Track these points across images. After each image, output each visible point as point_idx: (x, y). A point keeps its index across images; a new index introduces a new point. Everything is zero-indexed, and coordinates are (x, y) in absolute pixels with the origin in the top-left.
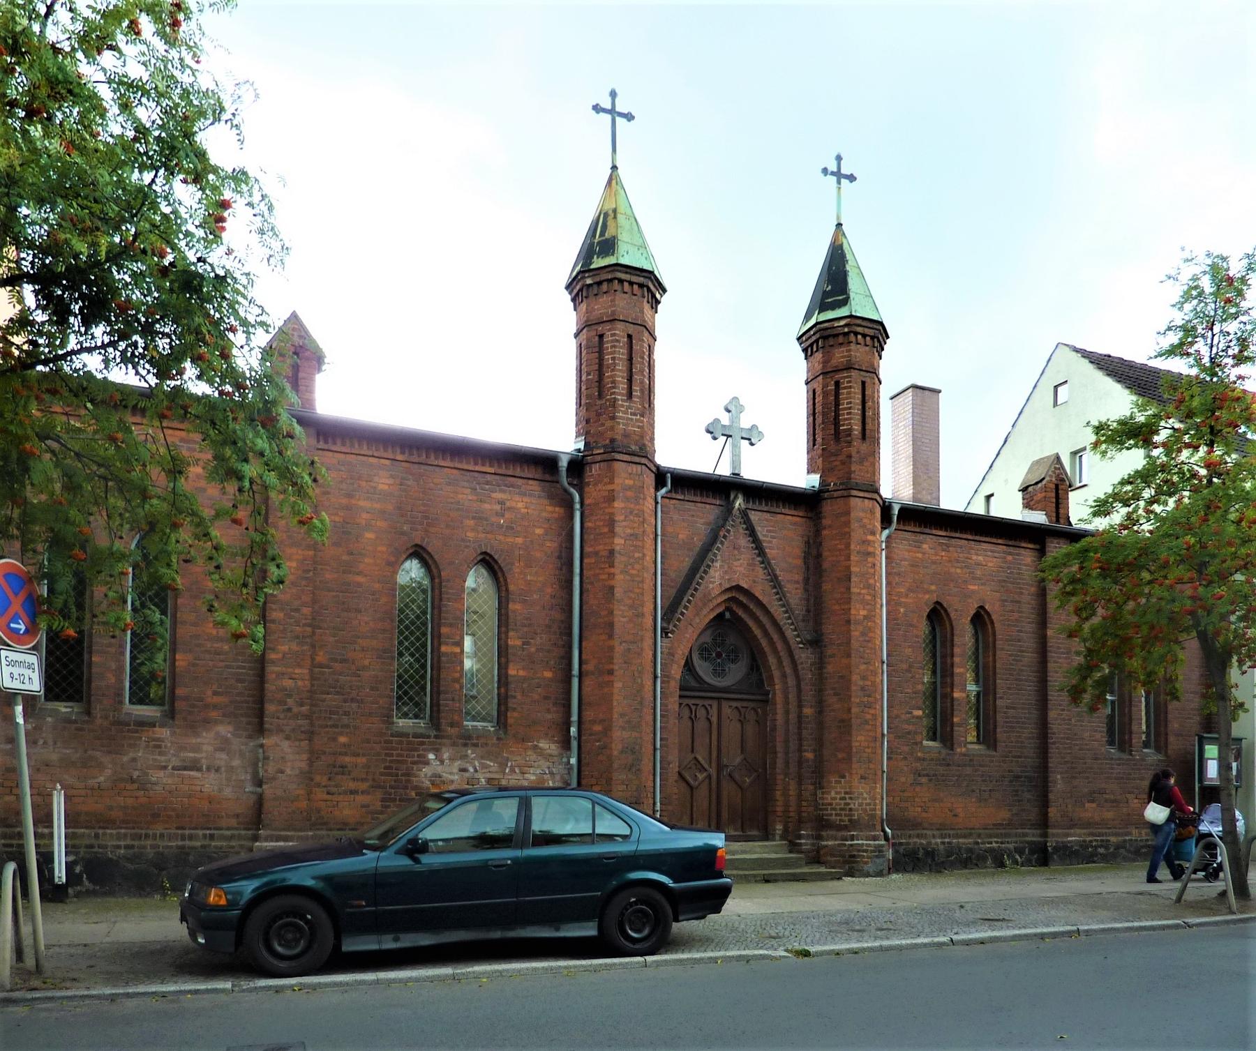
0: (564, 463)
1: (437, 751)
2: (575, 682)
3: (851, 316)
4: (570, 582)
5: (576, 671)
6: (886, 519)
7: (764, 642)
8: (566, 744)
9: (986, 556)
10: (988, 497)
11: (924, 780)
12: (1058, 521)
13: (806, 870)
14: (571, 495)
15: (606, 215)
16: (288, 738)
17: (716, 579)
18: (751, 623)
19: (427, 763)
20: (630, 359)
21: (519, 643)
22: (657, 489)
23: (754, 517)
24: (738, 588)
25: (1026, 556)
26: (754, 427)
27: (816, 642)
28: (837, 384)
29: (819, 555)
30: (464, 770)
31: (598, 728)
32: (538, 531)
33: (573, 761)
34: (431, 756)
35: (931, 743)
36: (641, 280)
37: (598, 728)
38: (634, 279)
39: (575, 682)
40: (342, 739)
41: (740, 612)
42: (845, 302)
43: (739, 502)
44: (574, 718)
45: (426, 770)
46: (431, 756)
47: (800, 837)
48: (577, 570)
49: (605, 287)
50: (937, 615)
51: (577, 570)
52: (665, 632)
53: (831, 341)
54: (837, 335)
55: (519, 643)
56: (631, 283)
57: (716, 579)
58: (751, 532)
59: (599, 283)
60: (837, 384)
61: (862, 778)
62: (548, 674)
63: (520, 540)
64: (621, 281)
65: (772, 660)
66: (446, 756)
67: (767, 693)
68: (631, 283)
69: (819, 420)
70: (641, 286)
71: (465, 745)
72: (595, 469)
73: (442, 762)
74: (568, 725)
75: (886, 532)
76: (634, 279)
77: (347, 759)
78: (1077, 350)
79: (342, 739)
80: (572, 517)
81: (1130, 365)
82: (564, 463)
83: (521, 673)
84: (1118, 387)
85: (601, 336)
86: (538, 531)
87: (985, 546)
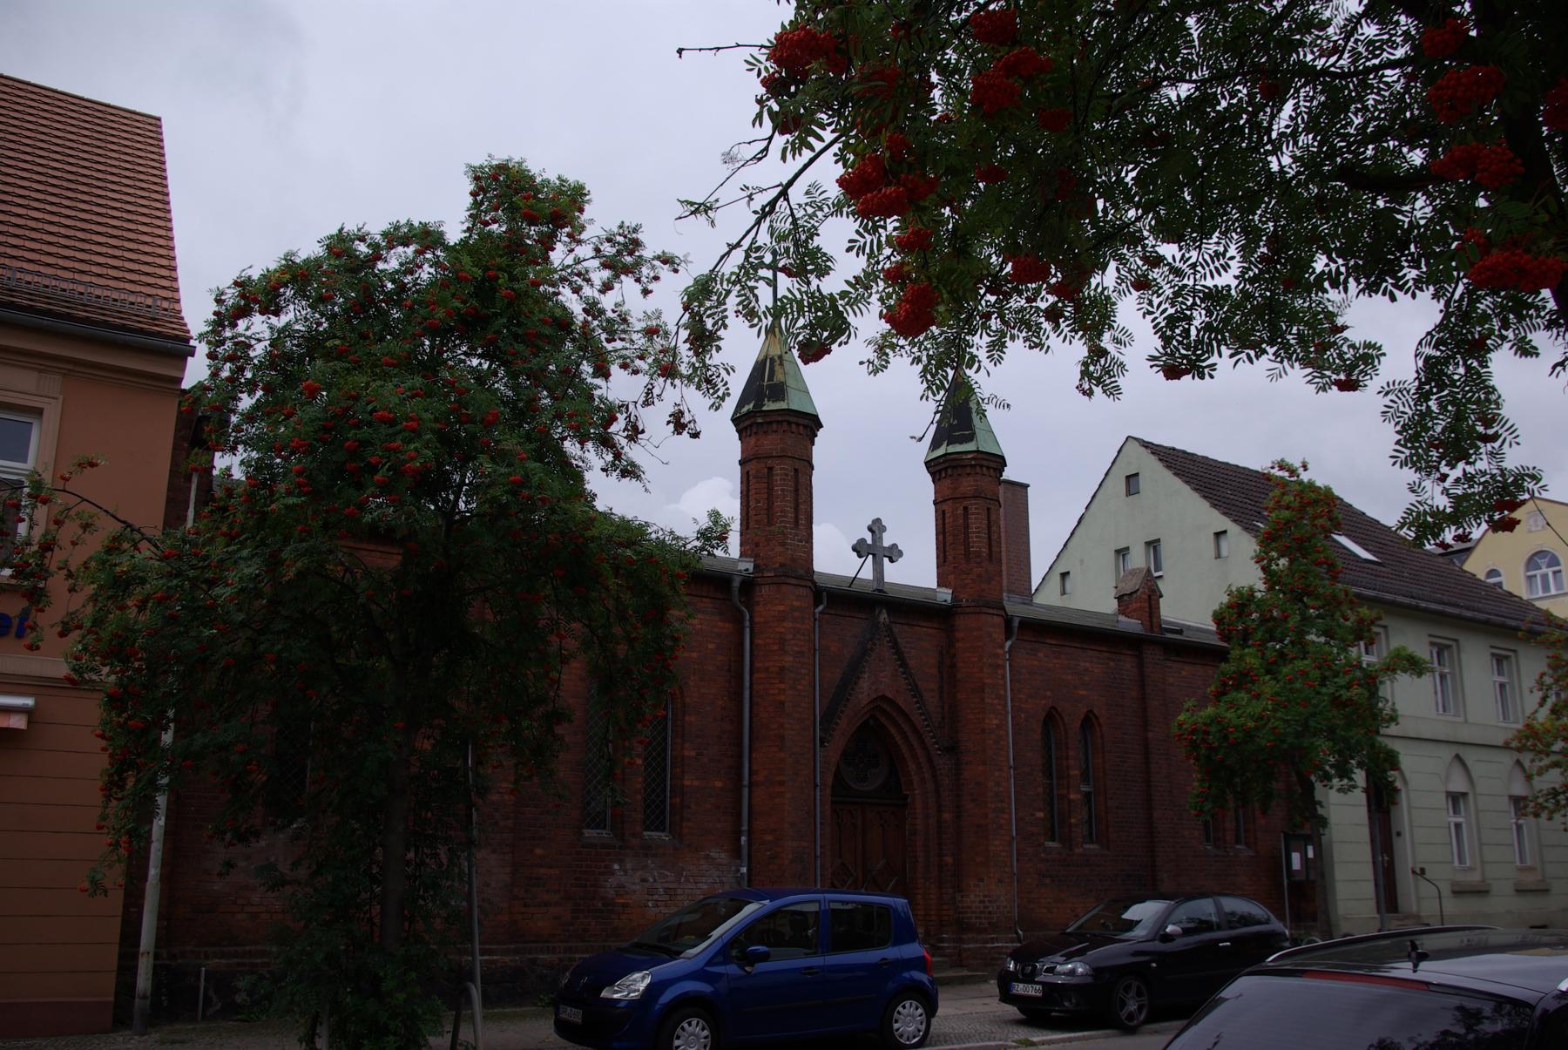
0: (736, 583)
1: (621, 862)
2: (746, 791)
3: (978, 452)
4: (740, 694)
5: (746, 782)
6: (1008, 633)
7: (904, 749)
8: (736, 852)
9: (1092, 664)
10: (1064, 575)
11: (1048, 881)
12: (1152, 629)
13: (951, 973)
14: (742, 613)
15: (772, 360)
16: (494, 852)
17: (865, 690)
18: (893, 730)
19: (613, 873)
20: (797, 490)
21: (693, 753)
22: (816, 606)
23: (896, 629)
24: (884, 698)
25: (1128, 664)
26: (894, 546)
27: (952, 749)
28: (965, 508)
29: (953, 666)
30: (644, 880)
31: (769, 838)
32: (711, 646)
33: (744, 870)
34: (616, 867)
35: (1051, 844)
36: (806, 422)
37: (769, 838)
38: (801, 421)
39: (746, 791)
40: (538, 851)
41: (883, 720)
42: (971, 438)
43: (884, 617)
44: (745, 828)
45: (612, 881)
46: (616, 867)
47: (942, 940)
48: (747, 684)
49: (775, 426)
50: (1051, 719)
51: (747, 684)
52: (822, 743)
53: (960, 471)
54: (964, 466)
55: (693, 753)
56: (798, 425)
57: (865, 690)
58: (895, 645)
59: (770, 423)
60: (965, 508)
61: (1000, 881)
62: (719, 784)
63: (695, 655)
64: (789, 423)
65: (912, 767)
66: (629, 866)
67: (906, 797)
68: (798, 425)
69: (950, 539)
70: (805, 427)
71: (646, 855)
72: (765, 590)
73: (626, 872)
74: (739, 833)
75: (1008, 644)
76: (801, 421)
77: (542, 871)
78: (1147, 445)
79: (538, 851)
80: (742, 635)
81: (1191, 457)
82: (736, 583)
83: (695, 783)
84: (1186, 489)
85: (770, 469)
86: (711, 646)
87: (1090, 653)
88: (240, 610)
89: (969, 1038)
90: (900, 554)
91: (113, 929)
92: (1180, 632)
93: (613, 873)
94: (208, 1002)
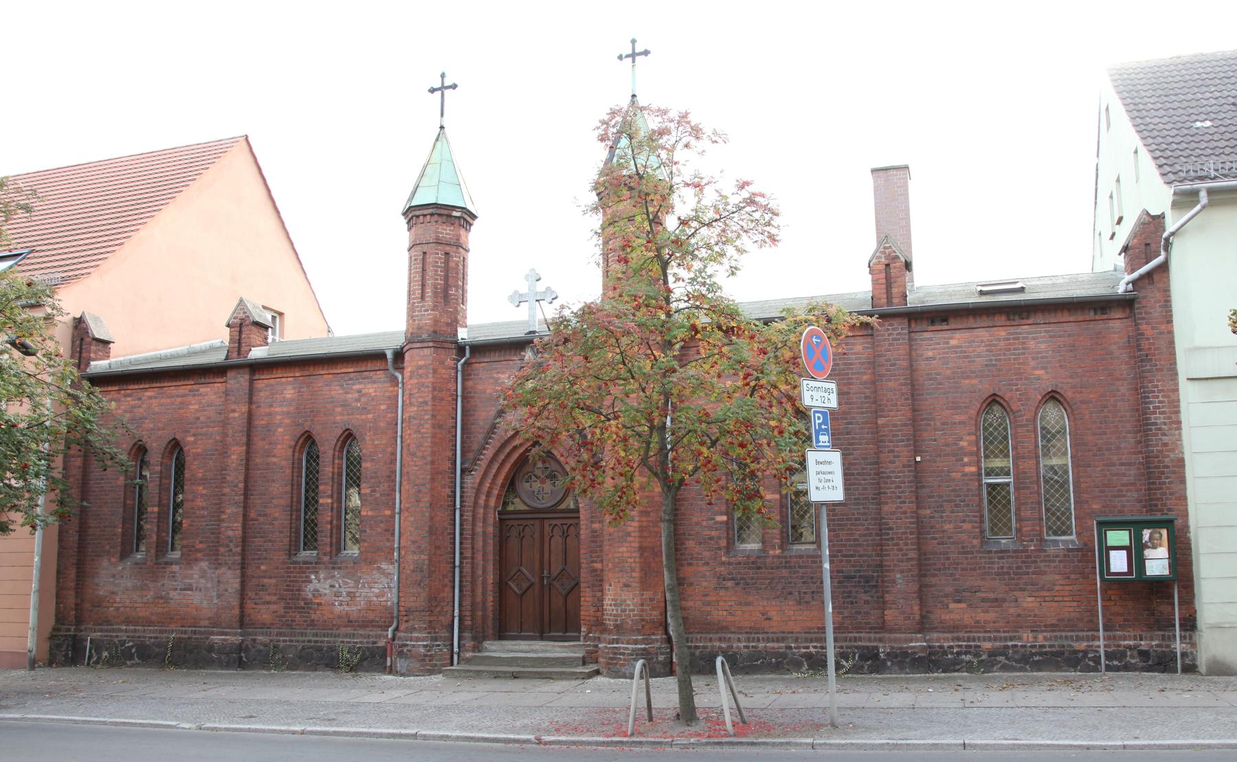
0: (389, 355)
1: (316, 573)
11: (729, 584)
14: (396, 378)
19: (311, 582)
21: (368, 491)
30: (332, 586)
36: (430, 211)
38: (425, 212)
45: (310, 587)
66: (322, 576)
76: (425, 212)
77: (265, 580)
79: (263, 567)
82: (389, 355)
83: (370, 513)
86: (383, 407)
88: (1048, 436)
89: (707, 744)
90: (511, 298)
91: (645, 700)
92: (1022, 290)
93: (311, 582)
94: (90, 657)
